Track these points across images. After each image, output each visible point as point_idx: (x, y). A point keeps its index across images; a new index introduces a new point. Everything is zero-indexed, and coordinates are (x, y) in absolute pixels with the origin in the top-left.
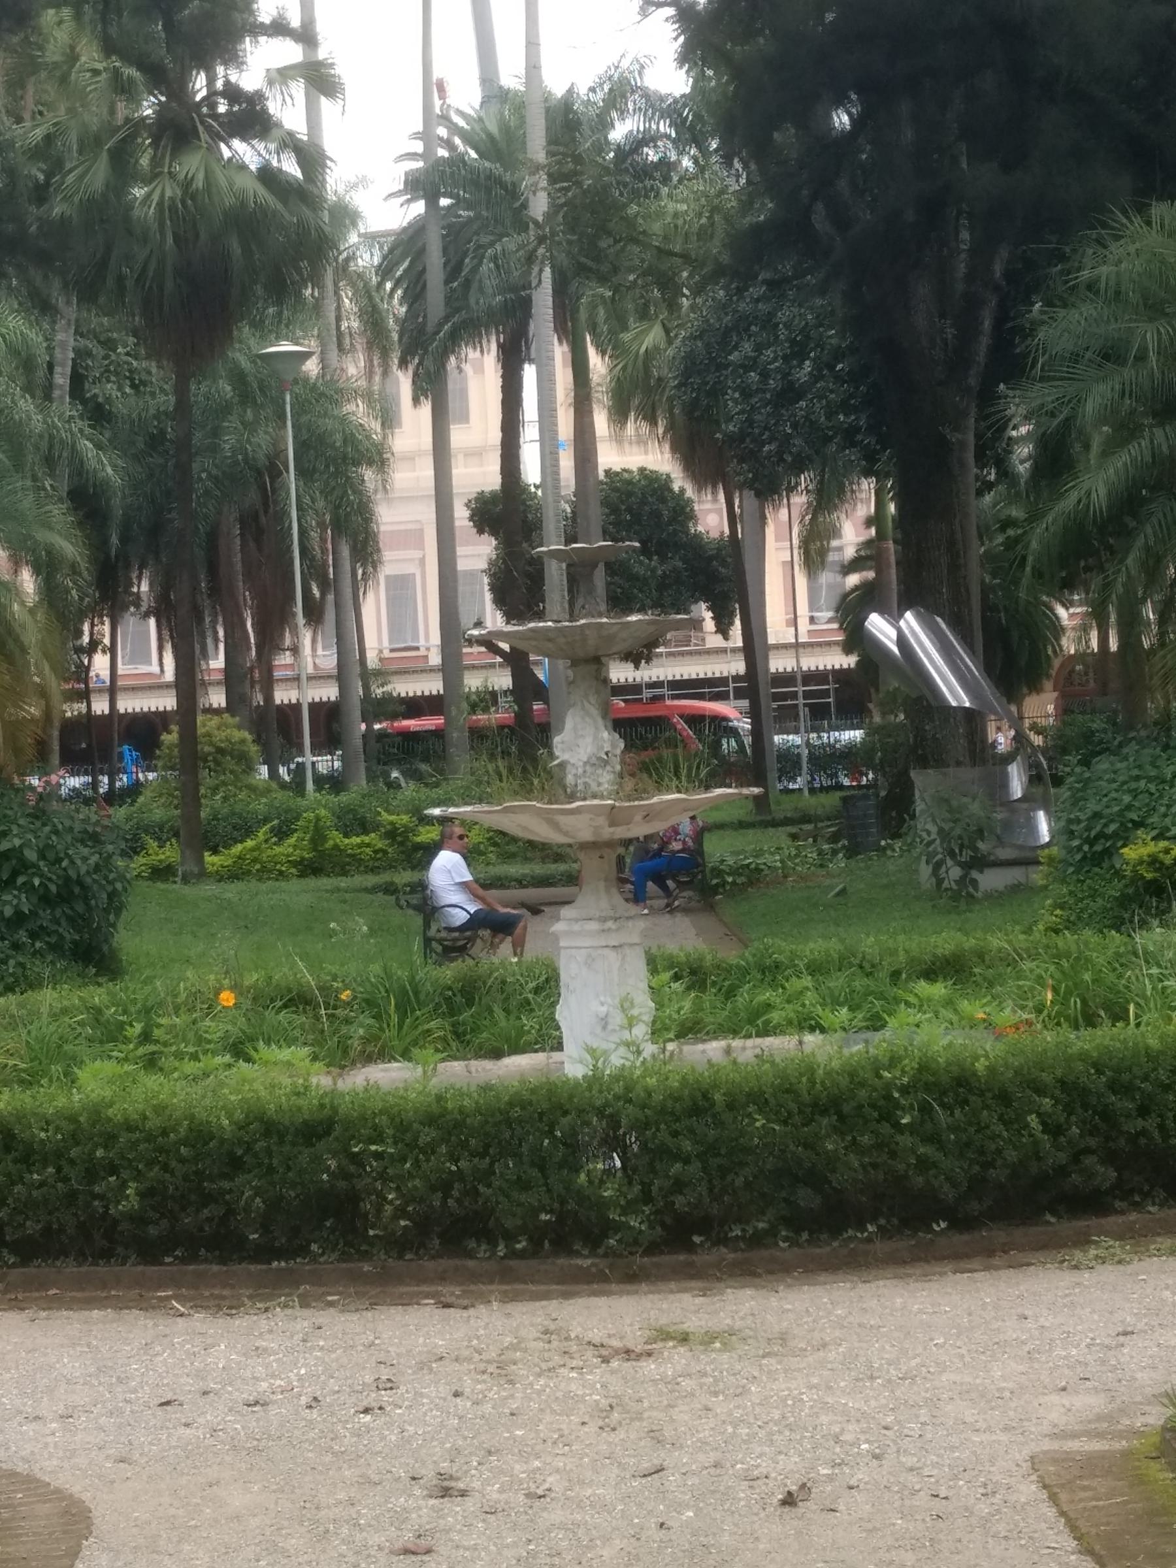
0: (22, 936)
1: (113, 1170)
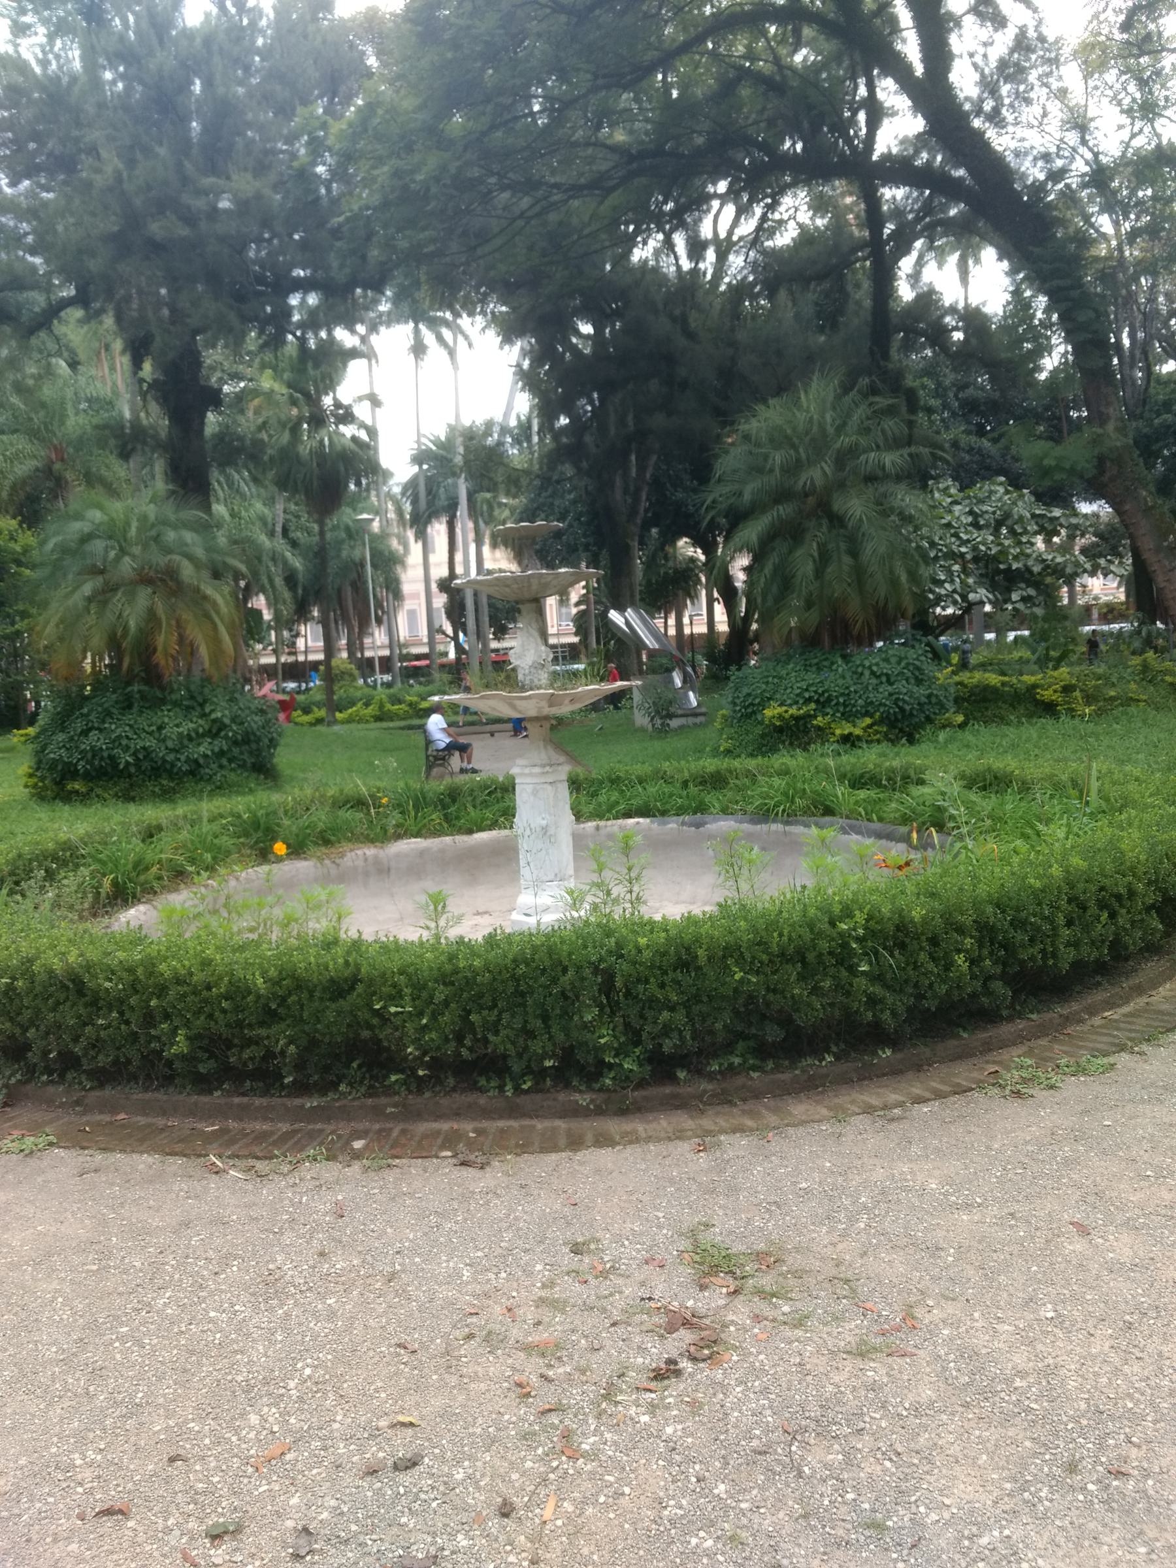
1: (167, 1016)
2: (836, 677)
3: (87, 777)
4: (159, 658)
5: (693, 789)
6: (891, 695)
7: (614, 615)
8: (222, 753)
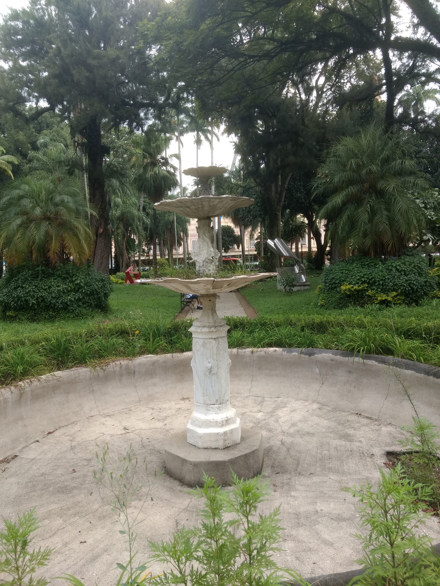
0: (80, 303)
2: (379, 271)
3: (15, 309)
4: (51, 254)
5: (307, 332)
6: (406, 281)
7: (270, 242)
8: (79, 300)
